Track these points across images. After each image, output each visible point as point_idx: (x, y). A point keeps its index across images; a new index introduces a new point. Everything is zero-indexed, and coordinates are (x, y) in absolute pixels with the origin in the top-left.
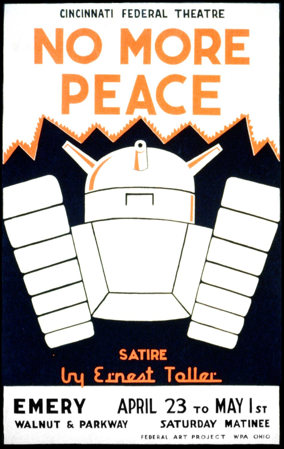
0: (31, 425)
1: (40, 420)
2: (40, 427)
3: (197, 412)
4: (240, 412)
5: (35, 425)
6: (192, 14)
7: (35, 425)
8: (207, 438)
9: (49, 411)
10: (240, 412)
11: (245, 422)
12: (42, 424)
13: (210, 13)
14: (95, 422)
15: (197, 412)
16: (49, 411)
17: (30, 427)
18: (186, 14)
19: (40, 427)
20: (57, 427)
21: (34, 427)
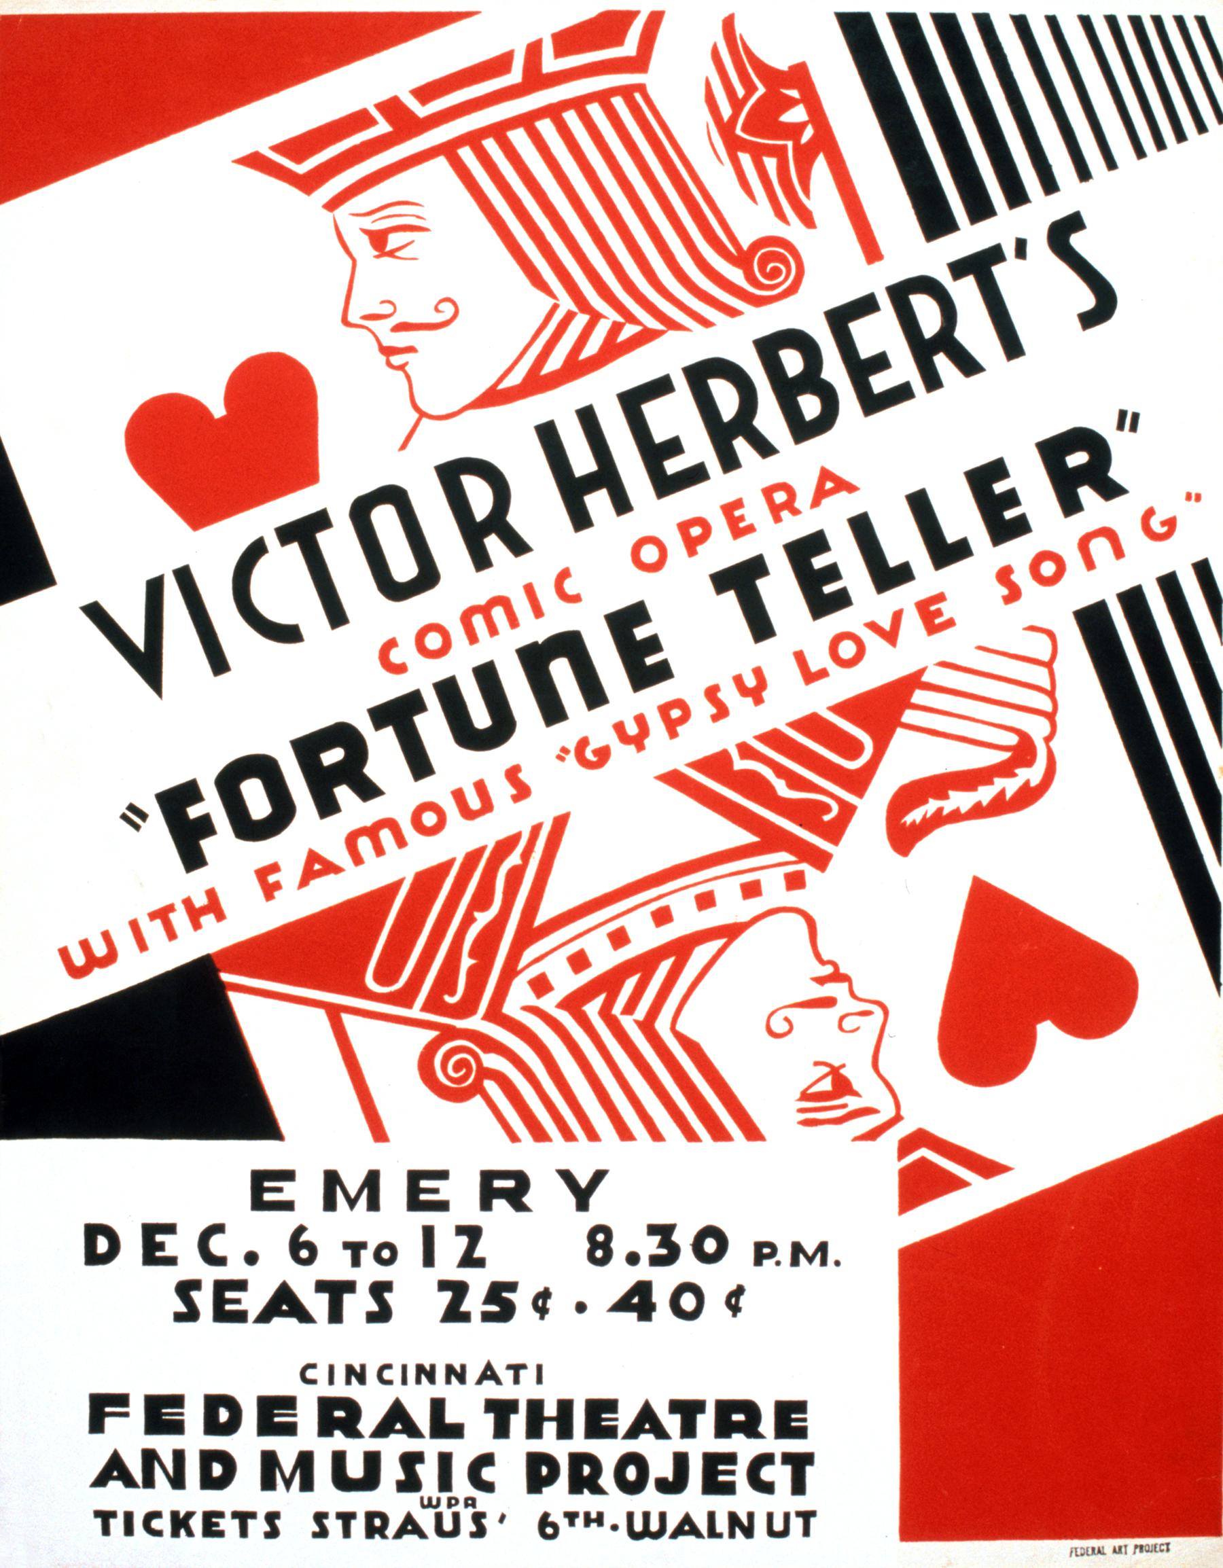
0: (703, 1526)
1: (362, 1387)
2: (732, 1535)
3: (106, 1531)
4: (1012, 347)
5: (814, 667)
6: (656, 454)
7: (814, 667)
8: (473, 1535)
9: (665, 485)
10: (1012, 347)
11: (323, 539)
12: (180, 1523)
13: (358, 1526)
14: (1053, 451)
15: (106, 1531)
16: (665, 485)
17: (698, 1534)
18: (591, 483)
19: (732, 1535)
20: (806, 1532)
21: (713, 1533)
